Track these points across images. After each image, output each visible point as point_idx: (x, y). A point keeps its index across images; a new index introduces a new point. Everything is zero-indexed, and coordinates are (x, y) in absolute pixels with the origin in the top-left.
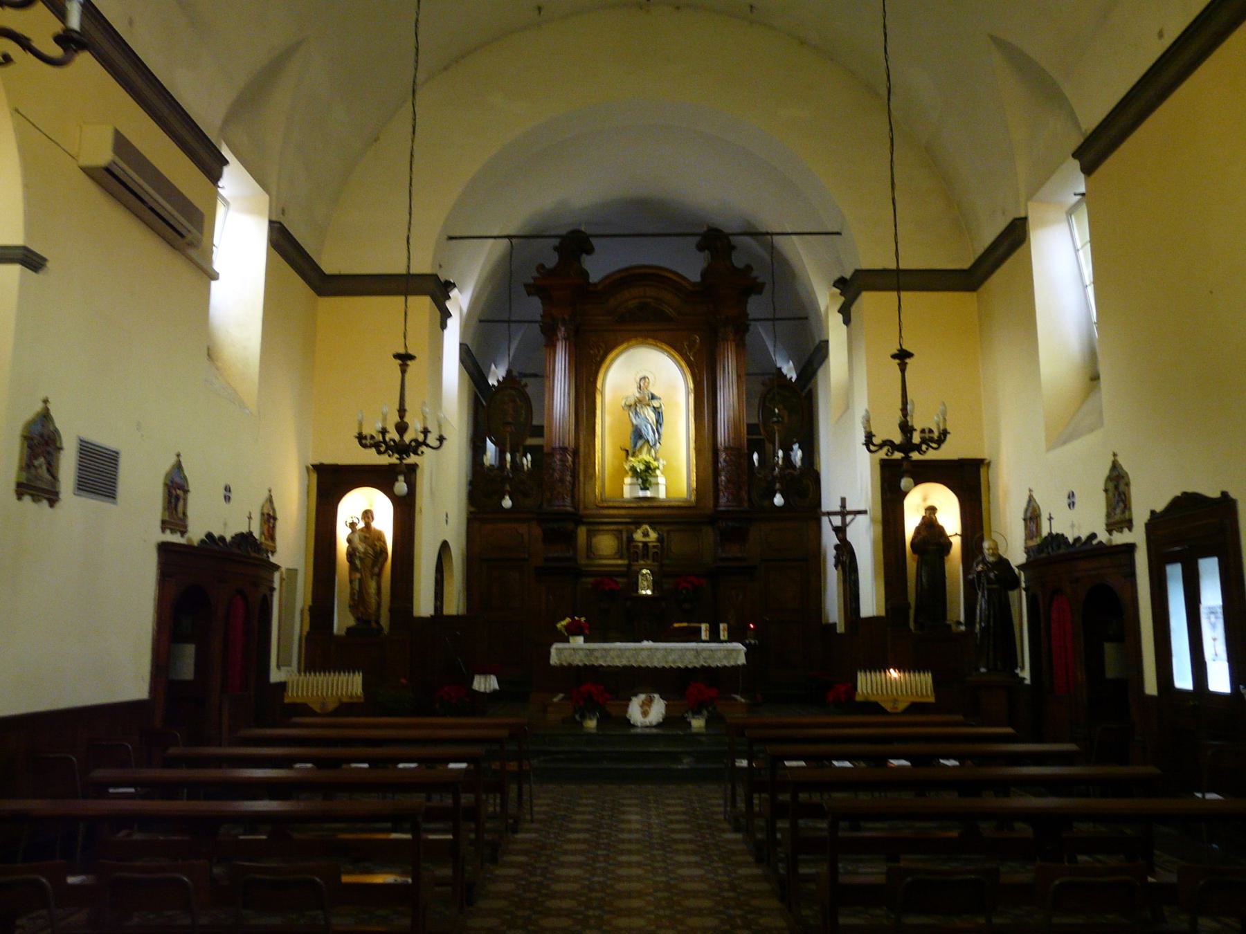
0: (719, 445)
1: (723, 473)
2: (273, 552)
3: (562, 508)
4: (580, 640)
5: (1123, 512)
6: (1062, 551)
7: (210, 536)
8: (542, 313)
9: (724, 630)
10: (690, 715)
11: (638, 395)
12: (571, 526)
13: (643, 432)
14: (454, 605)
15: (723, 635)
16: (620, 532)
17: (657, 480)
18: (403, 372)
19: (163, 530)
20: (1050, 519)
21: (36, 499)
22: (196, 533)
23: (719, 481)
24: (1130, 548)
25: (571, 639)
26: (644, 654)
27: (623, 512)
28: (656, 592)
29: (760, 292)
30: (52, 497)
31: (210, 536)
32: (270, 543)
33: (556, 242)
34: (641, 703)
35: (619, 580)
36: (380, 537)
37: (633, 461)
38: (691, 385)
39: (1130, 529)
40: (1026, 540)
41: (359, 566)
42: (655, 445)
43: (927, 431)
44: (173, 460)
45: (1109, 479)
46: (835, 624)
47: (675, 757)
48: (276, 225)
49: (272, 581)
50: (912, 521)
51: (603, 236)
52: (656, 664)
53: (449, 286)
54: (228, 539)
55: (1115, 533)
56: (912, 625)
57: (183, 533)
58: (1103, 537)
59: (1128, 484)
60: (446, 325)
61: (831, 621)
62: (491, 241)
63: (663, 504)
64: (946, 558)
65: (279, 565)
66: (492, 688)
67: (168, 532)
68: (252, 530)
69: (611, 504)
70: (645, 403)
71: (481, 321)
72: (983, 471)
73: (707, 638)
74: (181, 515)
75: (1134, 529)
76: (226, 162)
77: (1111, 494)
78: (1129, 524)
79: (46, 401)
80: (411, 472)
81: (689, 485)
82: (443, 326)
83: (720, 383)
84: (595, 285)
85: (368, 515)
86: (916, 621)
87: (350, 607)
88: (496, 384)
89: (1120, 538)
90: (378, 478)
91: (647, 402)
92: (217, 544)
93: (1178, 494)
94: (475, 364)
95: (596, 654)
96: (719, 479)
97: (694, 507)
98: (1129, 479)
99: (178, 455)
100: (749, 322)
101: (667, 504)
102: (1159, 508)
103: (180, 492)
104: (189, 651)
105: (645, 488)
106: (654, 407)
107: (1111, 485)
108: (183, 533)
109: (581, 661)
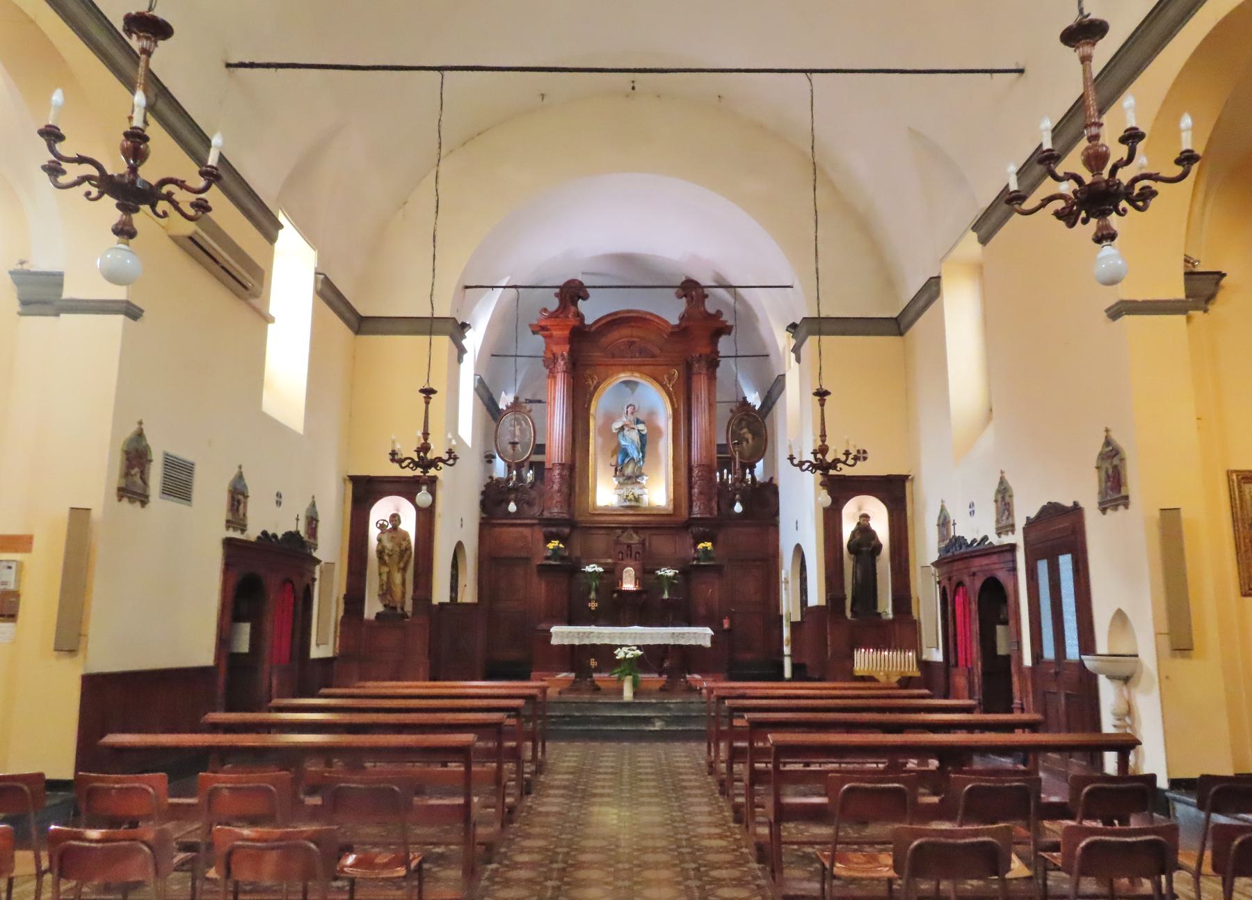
2: (315, 549)
5: (1007, 518)
6: (963, 550)
7: (265, 533)
14: (468, 595)
18: (427, 403)
19: (228, 528)
20: (954, 524)
21: (132, 501)
22: (252, 533)
24: (1012, 548)
29: (729, 333)
30: (143, 499)
31: (265, 533)
32: (311, 541)
33: (557, 290)
36: (405, 536)
39: (1013, 533)
40: (939, 542)
41: (387, 562)
43: (862, 452)
44: (236, 471)
45: (998, 491)
47: (648, 720)
48: (322, 277)
49: (314, 573)
50: (848, 528)
51: (594, 287)
53: (464, 326)
54: (280, 536)
55: (1003, 536)
56: (848, 614)
57: (243, 531)
58: (994, 540)
59: (1011, 496)
60: (462, 358)
62: (502, 289)
64: (877, 558)
65: (988, 245)
67: (231, 529)
68: (299, 529)
71: (493, 355)
72: (908, 485)
74: (241, 516)
75: (1016, 532)
76: (280, 226)
77: (999, 503)
78: (1011, 528)
79: (140, 423)
80: (432, 483)
82: (460, 360)
83: (694, 411)
84: (591, 326)
85: (395, 518)
86: (852, 610)
87: (379, 595)
88: (505, 408)
89: (1007, 539)
90: (407, 488)
92: (270, 540)
93: (1045, 503)
94: (487, 390)
97: (670, 515)
98: (1012, 491)
99: (240, 467)
100: (719, 359)
102: (1033, 515)
103: (241, 497)
104: (245, 629)
107: (999, 497)
108: (243, 531)
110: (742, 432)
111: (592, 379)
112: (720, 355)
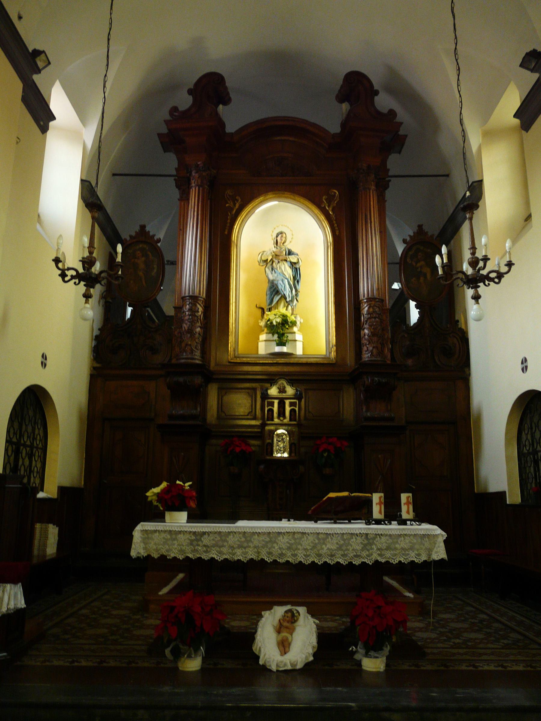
0: (361, 297)
1: (366, 326)
3: (190, 361)
4: (183, 516)
8: (177, 166)
9: (408, 503)
10: (361, 651)
11: (274, 250)
12: (198, 380)
13: (280, 287)
15: (406, 512)
16: (255, 389)
17: (295, 337)
23: (362, 335)
25: (168, 515)
26: (283, 541)
27: (257, 369)
28: (293, 455)
34: (276, 622)
35: (253, 442)
37: (270, 315)
38: (330, 238)
42: (292, 301)
46: (505, 492)
52: (301, 558)
61: (493, 488)
63: (299, 356)
66: (12, 606)
69: (245, 360)
70: (281, 258)
71: (114, 175)
73: (382, 517)
81: (328, 341)
84: (231, 134)
91: (284, 257)
95: (206, 540)
96: (362, 333)
101: (304, 361)
105: (281, 343)
106: (291, 262)
109: (182, 551)
110: (418, 265)
111: (234, 201)
112: (390, 173)
